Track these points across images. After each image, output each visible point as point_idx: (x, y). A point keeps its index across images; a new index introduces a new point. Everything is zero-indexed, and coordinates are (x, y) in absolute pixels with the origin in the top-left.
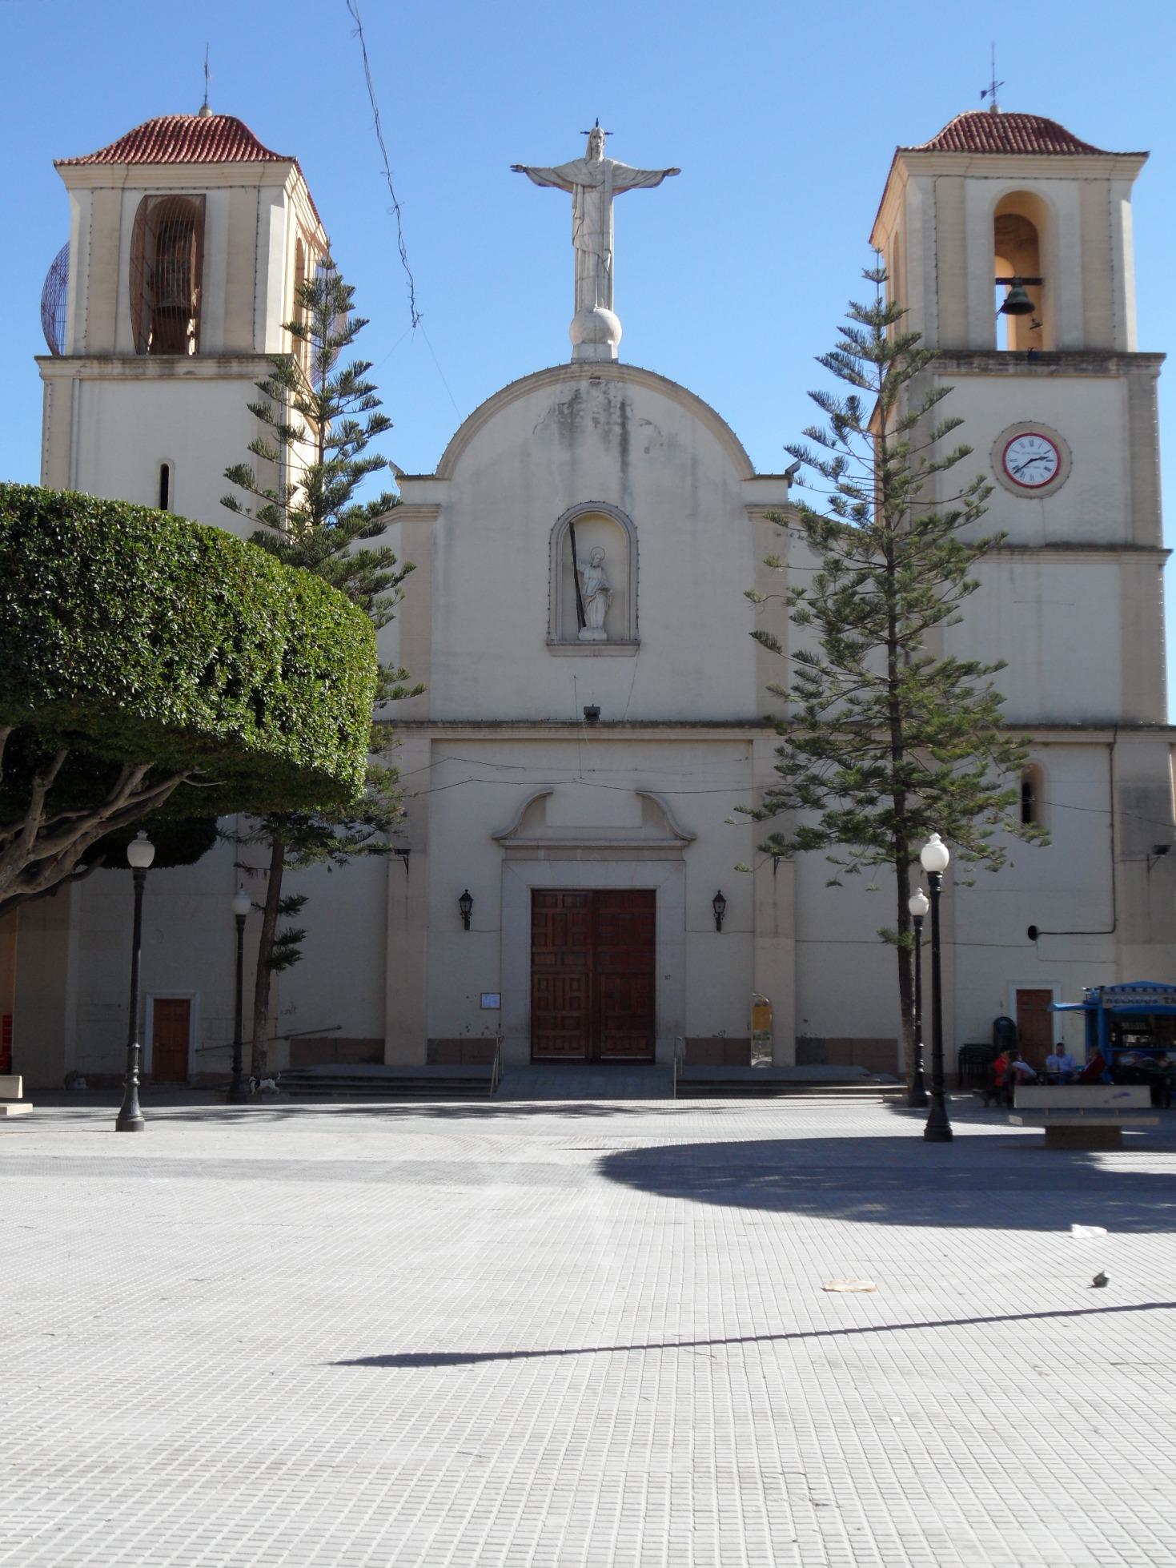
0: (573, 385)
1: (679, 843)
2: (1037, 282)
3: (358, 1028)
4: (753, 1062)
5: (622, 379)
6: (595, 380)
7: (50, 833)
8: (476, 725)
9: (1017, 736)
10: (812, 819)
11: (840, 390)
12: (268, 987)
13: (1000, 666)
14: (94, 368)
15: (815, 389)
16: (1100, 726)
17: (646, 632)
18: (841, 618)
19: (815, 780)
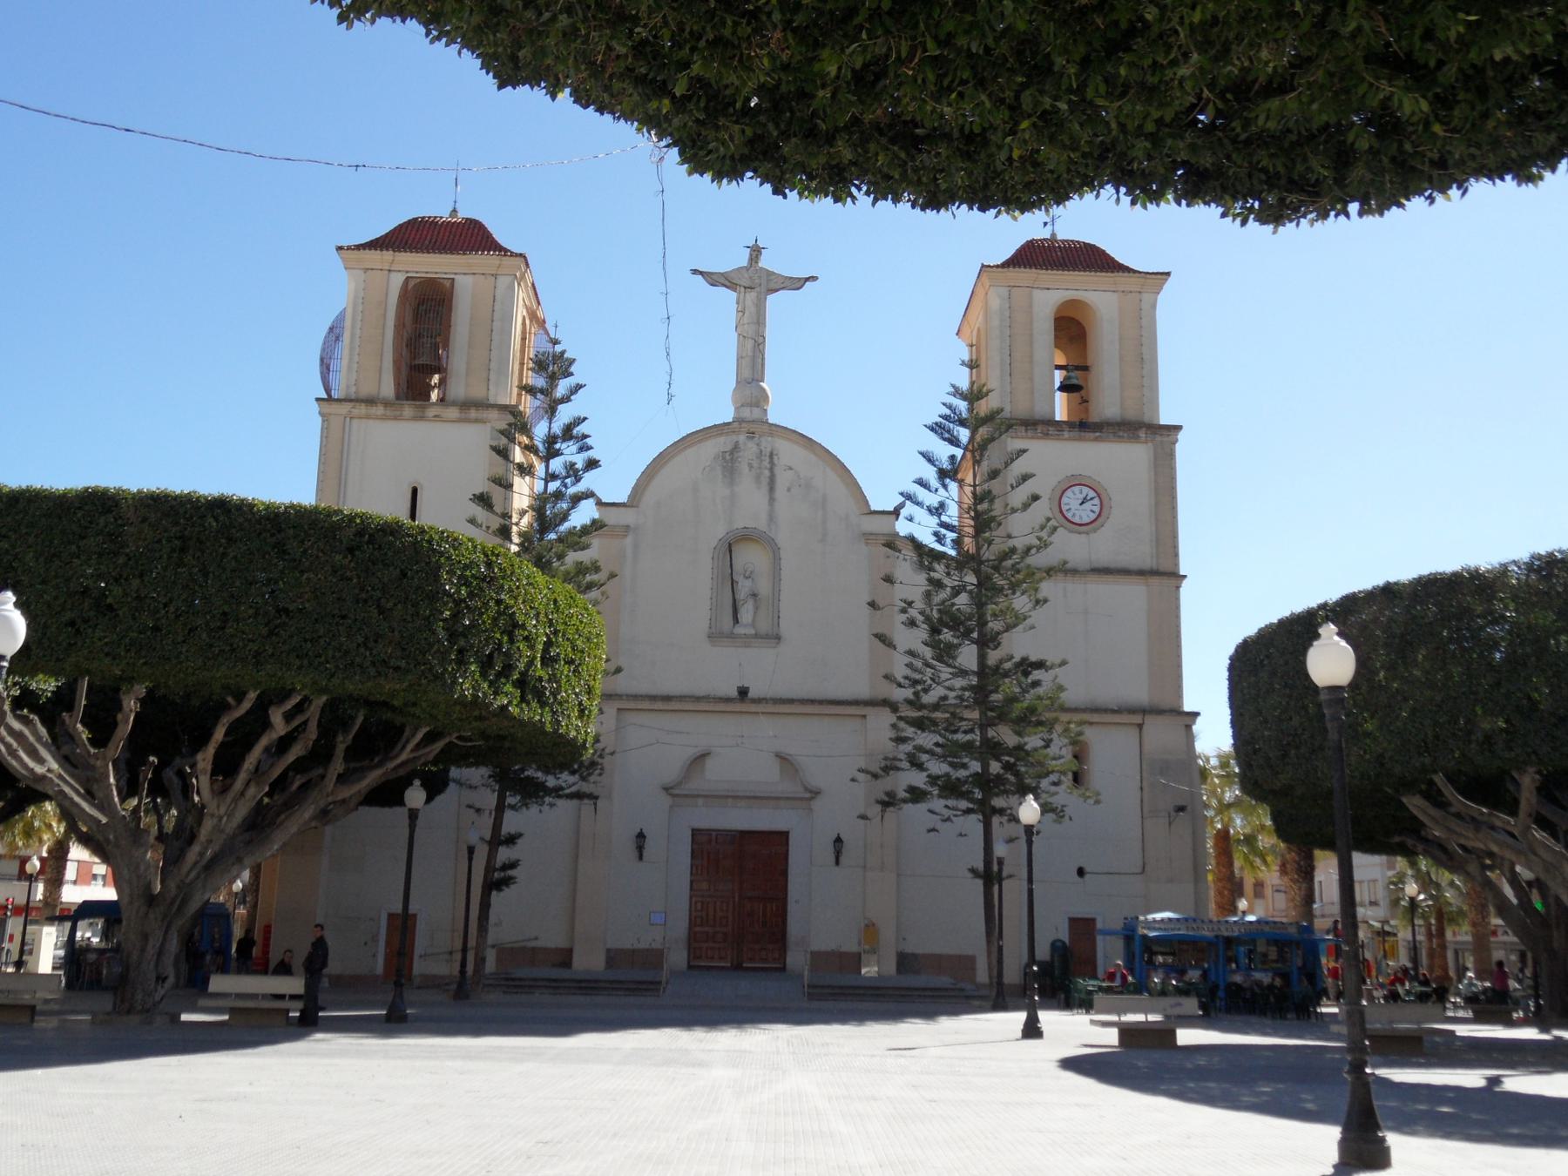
0: (734, 438)
1: (808, 795)
2: (1085, 368)
3: (552, 938)
4: (863, 971)
5: (771, 435)
6: (751, 434)
7: (342, 779)
8: (653, 698)
9: (1077, 717)
10: (918, 779)
11: (944, 451)
12: (489, 905)
13: (1063, 663)
14: (362, 409)
15: (923, 449)
16: (1132, 711)
17: (785, 628)
18: (944, 626)
19: (921, 749)
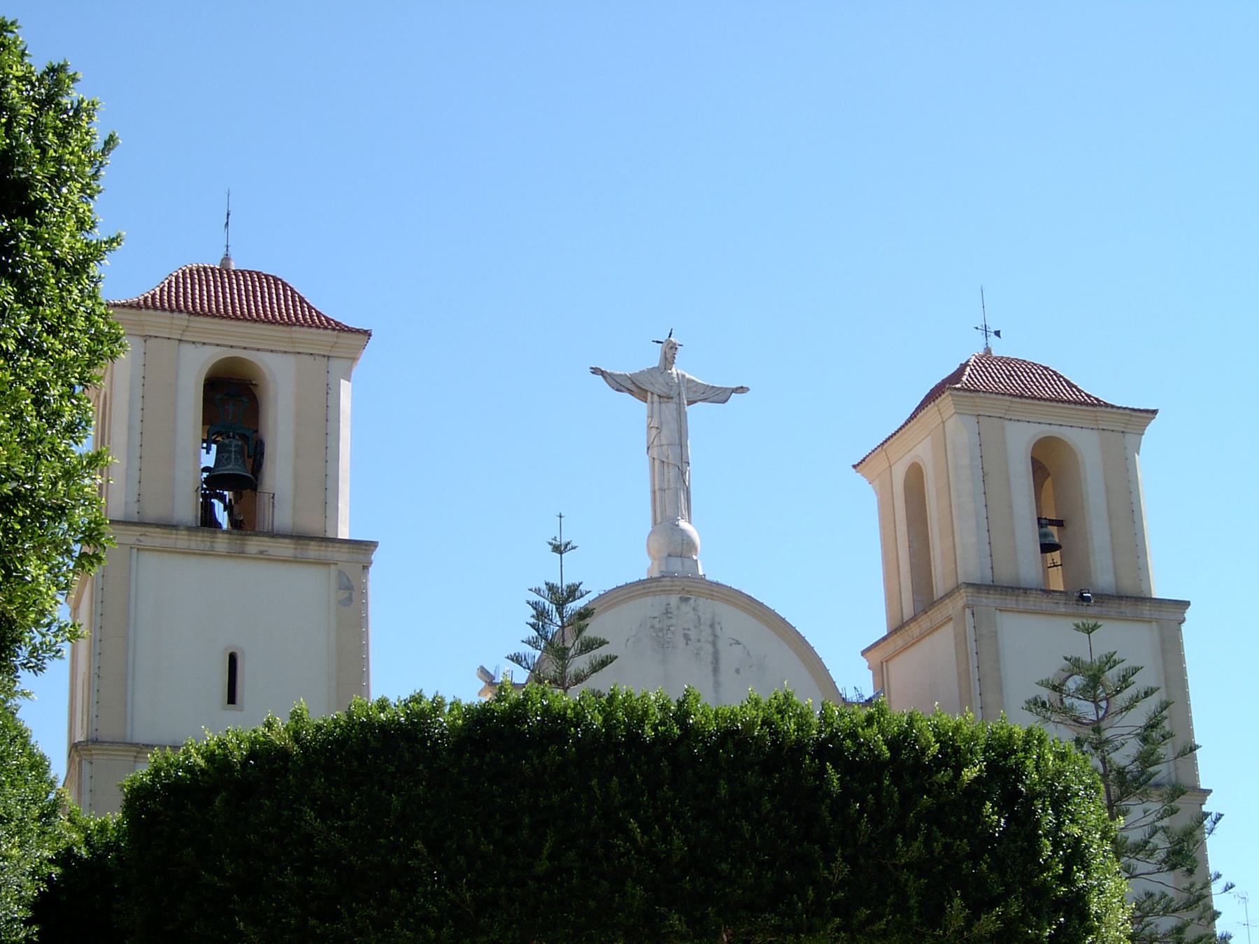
14: (157, 538)
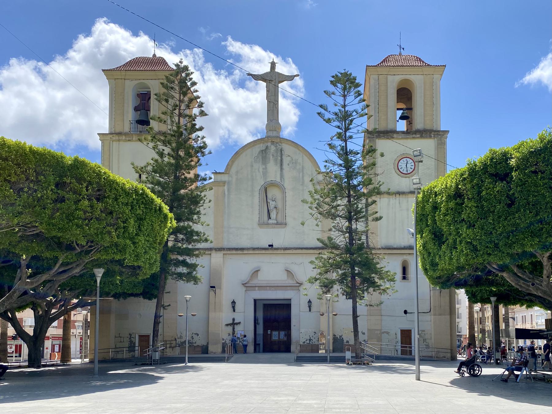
1: (298, 285)
14: (117, 138)
17: (289, 220)
